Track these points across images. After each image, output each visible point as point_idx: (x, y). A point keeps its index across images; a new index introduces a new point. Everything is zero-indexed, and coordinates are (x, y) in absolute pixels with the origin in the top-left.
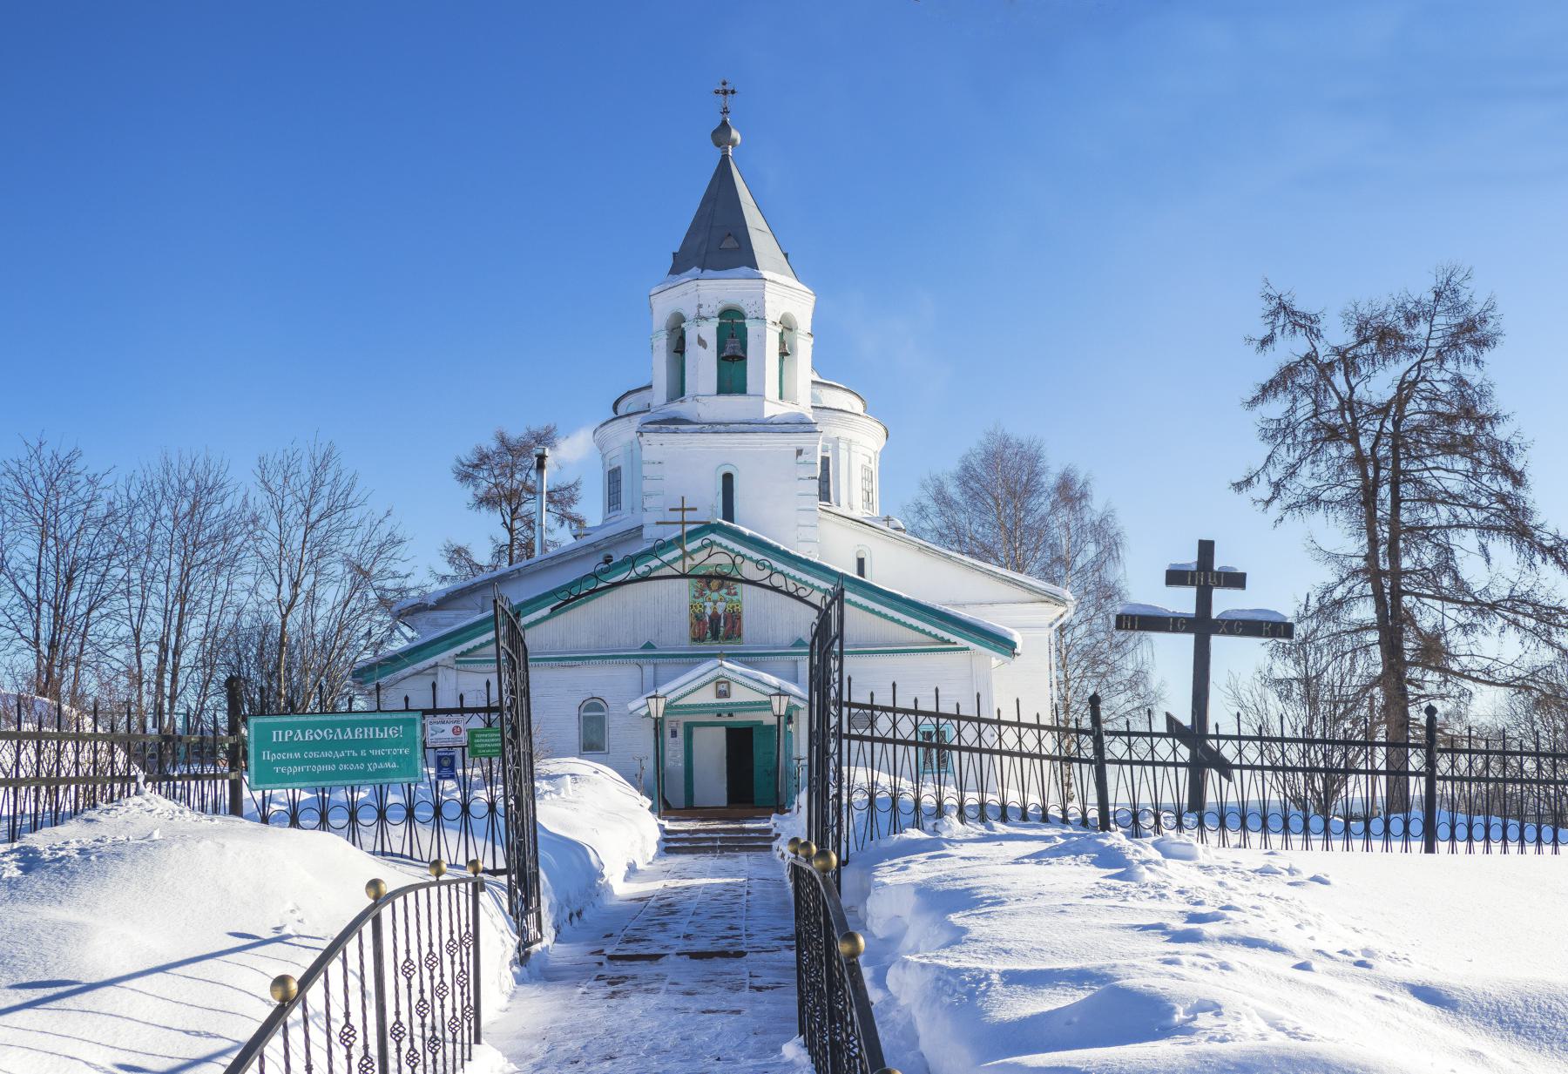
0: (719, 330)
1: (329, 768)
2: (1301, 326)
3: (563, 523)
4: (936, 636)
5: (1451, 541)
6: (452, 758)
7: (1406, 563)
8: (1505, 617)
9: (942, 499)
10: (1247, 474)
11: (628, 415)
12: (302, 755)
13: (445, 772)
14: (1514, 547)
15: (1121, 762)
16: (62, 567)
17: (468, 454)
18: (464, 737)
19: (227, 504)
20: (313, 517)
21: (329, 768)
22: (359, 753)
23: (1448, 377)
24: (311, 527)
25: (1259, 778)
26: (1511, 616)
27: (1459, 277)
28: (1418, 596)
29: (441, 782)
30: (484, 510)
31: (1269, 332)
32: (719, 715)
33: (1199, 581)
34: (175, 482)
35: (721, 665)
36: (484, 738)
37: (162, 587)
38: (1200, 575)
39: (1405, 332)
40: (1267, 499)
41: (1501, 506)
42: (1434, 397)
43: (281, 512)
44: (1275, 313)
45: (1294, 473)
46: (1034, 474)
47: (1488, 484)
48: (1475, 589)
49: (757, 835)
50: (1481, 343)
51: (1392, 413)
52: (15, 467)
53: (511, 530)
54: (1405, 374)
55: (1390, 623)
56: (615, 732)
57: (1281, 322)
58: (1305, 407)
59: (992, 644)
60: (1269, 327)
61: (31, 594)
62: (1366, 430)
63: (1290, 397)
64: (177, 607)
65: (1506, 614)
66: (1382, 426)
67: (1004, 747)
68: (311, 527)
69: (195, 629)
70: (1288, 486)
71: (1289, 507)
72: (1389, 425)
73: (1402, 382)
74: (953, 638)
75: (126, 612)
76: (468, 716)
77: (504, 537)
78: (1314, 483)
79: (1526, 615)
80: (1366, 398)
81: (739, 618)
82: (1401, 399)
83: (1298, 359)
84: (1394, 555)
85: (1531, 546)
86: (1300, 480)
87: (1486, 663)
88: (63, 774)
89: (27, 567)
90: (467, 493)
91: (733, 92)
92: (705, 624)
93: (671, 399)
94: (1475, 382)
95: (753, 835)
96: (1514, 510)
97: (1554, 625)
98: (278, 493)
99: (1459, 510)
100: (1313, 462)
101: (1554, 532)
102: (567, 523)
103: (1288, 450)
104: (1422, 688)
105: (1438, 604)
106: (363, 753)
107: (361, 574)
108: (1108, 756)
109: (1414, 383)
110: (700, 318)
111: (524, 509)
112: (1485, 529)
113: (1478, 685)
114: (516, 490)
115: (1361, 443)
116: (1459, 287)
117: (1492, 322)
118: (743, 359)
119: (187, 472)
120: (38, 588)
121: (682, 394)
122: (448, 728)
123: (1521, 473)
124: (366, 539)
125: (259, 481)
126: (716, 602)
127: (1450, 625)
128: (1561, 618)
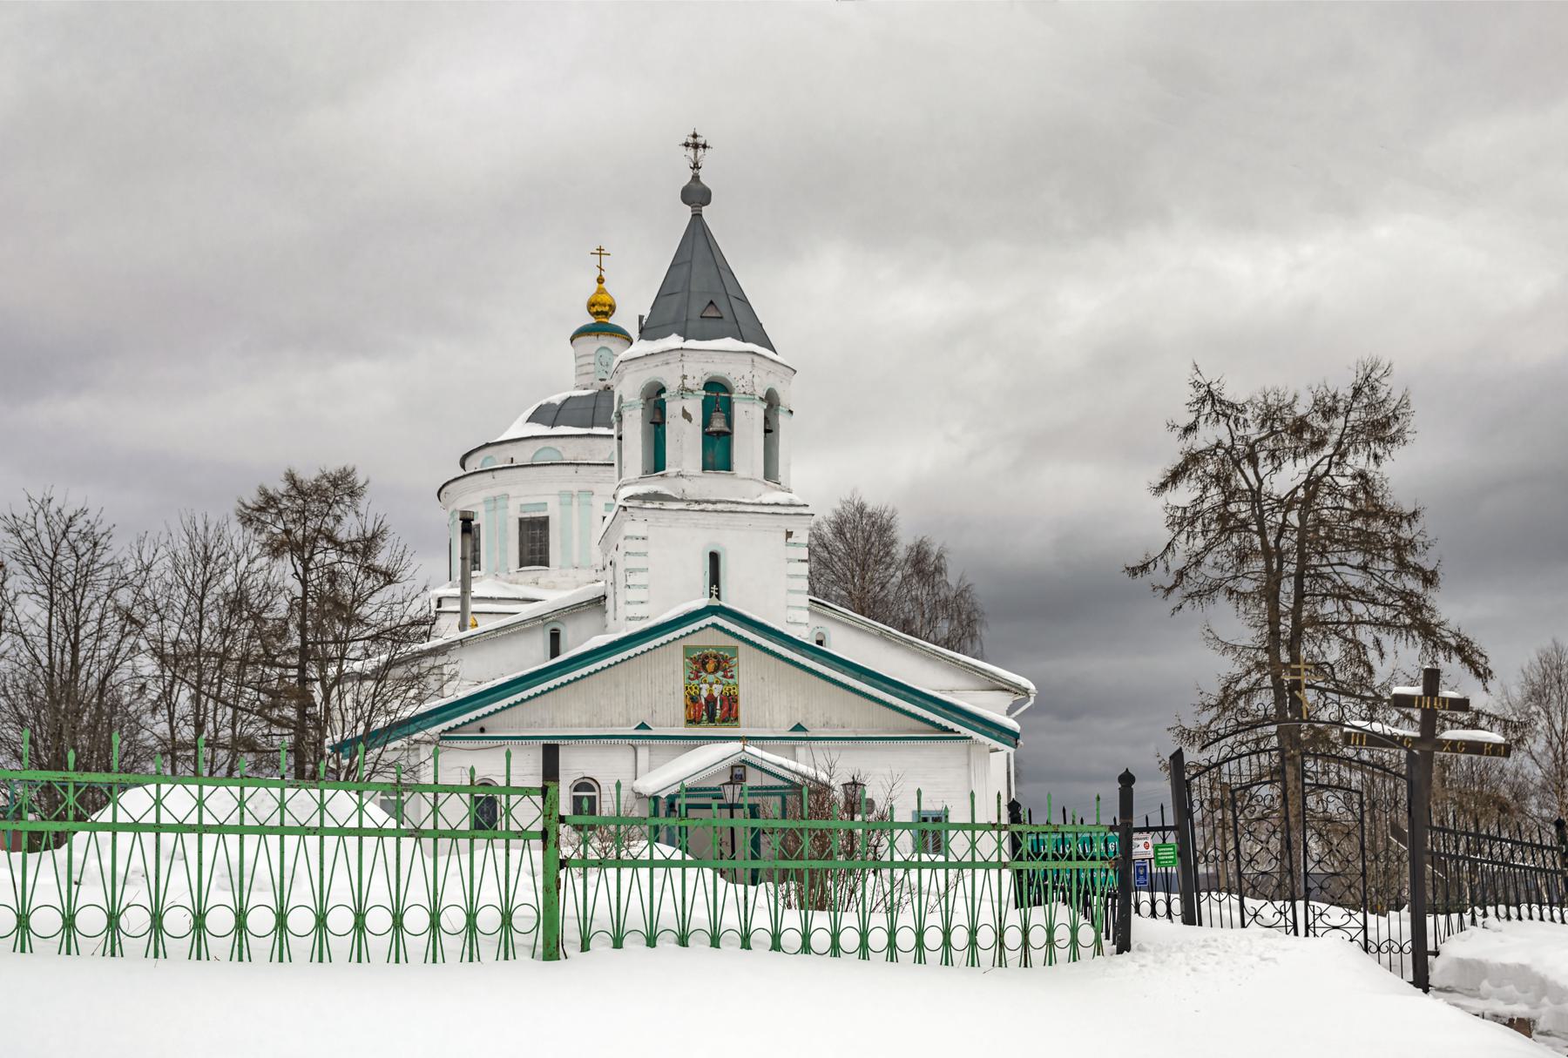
0: (706, 404)
2: (1225, 415)
17: (252, 498)
23: (1349, 471)
25: (501, 852)
27: (1379, 372)
33: (1426, 704)
35: (743, 750)
38: (1426, 699)
40: (1168, 585)
43: (354, 584)
44: (1203, 401)
46: (888, 545)
47: (1392, 581)
53: (304, 583)
55: (1289, 715)
59: (996, 734)
63: (1200, 485)
67: (969, 833)
70: (1192, 574)
71: (1190, 596)
72: (1293, 518)
74: (957, 727)
81: (736, 701)
85: (1435, 645)
86: (1202, 569)
91: (705, 146)
92: (701, 705)
101: (1455, 630)
110: (684, 391)
116: (1377, 384)
123: (1434, 573)
126: (711, 686)
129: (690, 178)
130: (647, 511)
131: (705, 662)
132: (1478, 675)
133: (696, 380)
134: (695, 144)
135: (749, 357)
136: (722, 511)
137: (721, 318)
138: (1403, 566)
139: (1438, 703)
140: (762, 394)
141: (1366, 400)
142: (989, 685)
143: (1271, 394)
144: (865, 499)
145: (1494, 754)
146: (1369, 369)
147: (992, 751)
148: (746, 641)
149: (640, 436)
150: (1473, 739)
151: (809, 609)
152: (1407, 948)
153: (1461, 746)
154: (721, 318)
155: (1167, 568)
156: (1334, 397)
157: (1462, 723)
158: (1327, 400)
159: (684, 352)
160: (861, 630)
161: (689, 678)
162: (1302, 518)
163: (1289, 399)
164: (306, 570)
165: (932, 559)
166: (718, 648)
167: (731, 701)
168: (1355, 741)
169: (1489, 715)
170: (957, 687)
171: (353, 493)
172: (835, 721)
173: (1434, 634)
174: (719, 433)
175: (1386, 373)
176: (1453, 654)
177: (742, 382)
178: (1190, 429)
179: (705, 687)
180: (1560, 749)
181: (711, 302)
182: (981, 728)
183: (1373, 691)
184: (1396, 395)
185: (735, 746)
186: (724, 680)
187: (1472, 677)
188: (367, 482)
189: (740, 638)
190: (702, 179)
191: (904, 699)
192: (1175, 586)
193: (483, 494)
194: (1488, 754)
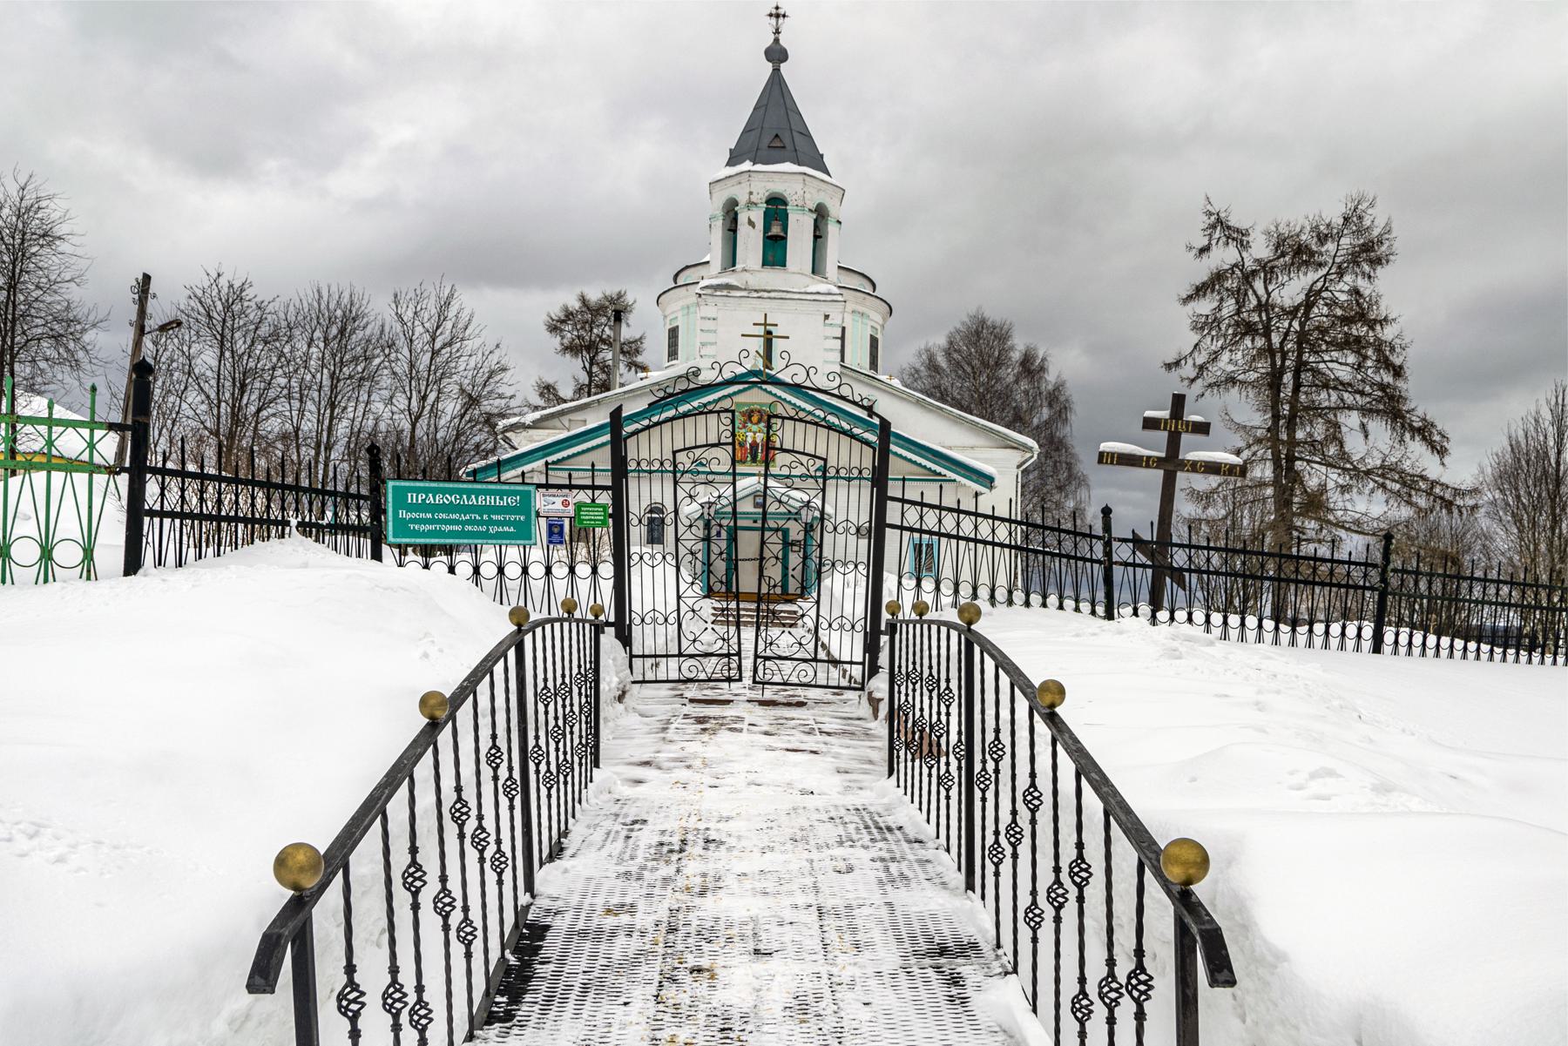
1: (456, 528)
2: (1233, 239)
3: (630, 370)
4: (930, 469)
5: (1339, 420)
6: (562, 526)
7: (1300, 435)
8: (1376, 482)
9: (933, 366)
10: (1177, 357)
12: (433, 515)
13: (555, 538)
14: (1389, 427)
15: (1126, 564)
16: (237, 375)
17: (557, 312)
18: (571, 510)
19: (368, 331)
20: (438, 345)
21: (456, 528)
23: (1346, 288)
24: (435, 353)
26: (1380, 480)
28: (1308, 462)
29: (551, 546)
30: (568, 356)
31: (1207, 243)
37: (316, 394)
39: (1315, 249)
40: (1192, 377)
41: (1380, 393)
42: (1332, 303)
43: (411, 340)
44: (1213, 227)
45: (1216, 358)
46: (1005, 351)
48: (1355, 458)
50: (1377, 262)
51: (1299, 315)
52: (199, 293)
53: (590, 374)
54: (1312, 285)
57: (1217, 235)
58: (1230, 306)
59: (975, 478)
60: (1207, 237)
61: (213, 395)
62: (1278, 328)
63: (1218, 298)
64: (328, 411)
65: (1377, 479)
66: (1290, 325)
68: (435, 353)
69: (342, 428)
70: (1210, 368)
71: (1210, 386)
72: (1296, 324)
73: (1310, 290)
74: (944, 471)
75: (288, 414)
76: (575, 491)
77: (584, 379)
78: (1231, 368)
79: (1393, 480)
80: (1278, 302)
82: (1309, 305)
83: (1227, 267)
84: (1291, 428)
85: (1403, 426)
87: (1357, 516)
88: (223, 513)
89: (209, 373)
90: (556, 341)
91: (784, 16)
93: (724, 270)
94: (1366, 293)
96: (1392, 398)
97: (1415, 489)
99: (1346, 395)
100: (1231, 351)
101: (1422, 416)
102: (633, 369)
103: (1212, 340)
104: (1304, 534)
105: (1323, 469)
106: (485, 517)
107: (472, 401)
108: (1115, 558)
109: (1320, 291)
110: (751, 204)
111: (601, 356)
112: (1366, 411)
113: (1349, 533)
114: (594, 342)
115: (1273, 337)
117: (1387, 244)
118: (784, 239)
120: (219, 390)
121: (734, 265)
122: (559, 500)
123: (1401, 367)
124: (479, 366)
125: (393, 315)
127: (1331, 485)
128: (1421, 484)
129: (772, 41)
133: (760, 196)
134: (777, 15)
135: (802, 177)
137: (784, 147)
140: (813, 207)
141: (1354, 228)
142: (1003, 444)
144: (987, 315)
145: (1230, 474)
149: (720, 241)
150: (1212, 460)
152: (858, 627)
153: (1201, 466)
154: (784, 147)
155: (1194, 364)
158: (1322, 228)
160: (902, 398)
164: (591, 364)
165: (1038, 361)
166: (761, 405)
169: (1442, 485)
173: (1403, 417)
175: (1372, 205)
177: (795, 197)
178: (1204, 250)
179: (750, 435)
181: (777, 136)
183: (1352, 463)
188: (635, 302)
190: (781, 42)
193: (681, 303)
194: (1224, 475)
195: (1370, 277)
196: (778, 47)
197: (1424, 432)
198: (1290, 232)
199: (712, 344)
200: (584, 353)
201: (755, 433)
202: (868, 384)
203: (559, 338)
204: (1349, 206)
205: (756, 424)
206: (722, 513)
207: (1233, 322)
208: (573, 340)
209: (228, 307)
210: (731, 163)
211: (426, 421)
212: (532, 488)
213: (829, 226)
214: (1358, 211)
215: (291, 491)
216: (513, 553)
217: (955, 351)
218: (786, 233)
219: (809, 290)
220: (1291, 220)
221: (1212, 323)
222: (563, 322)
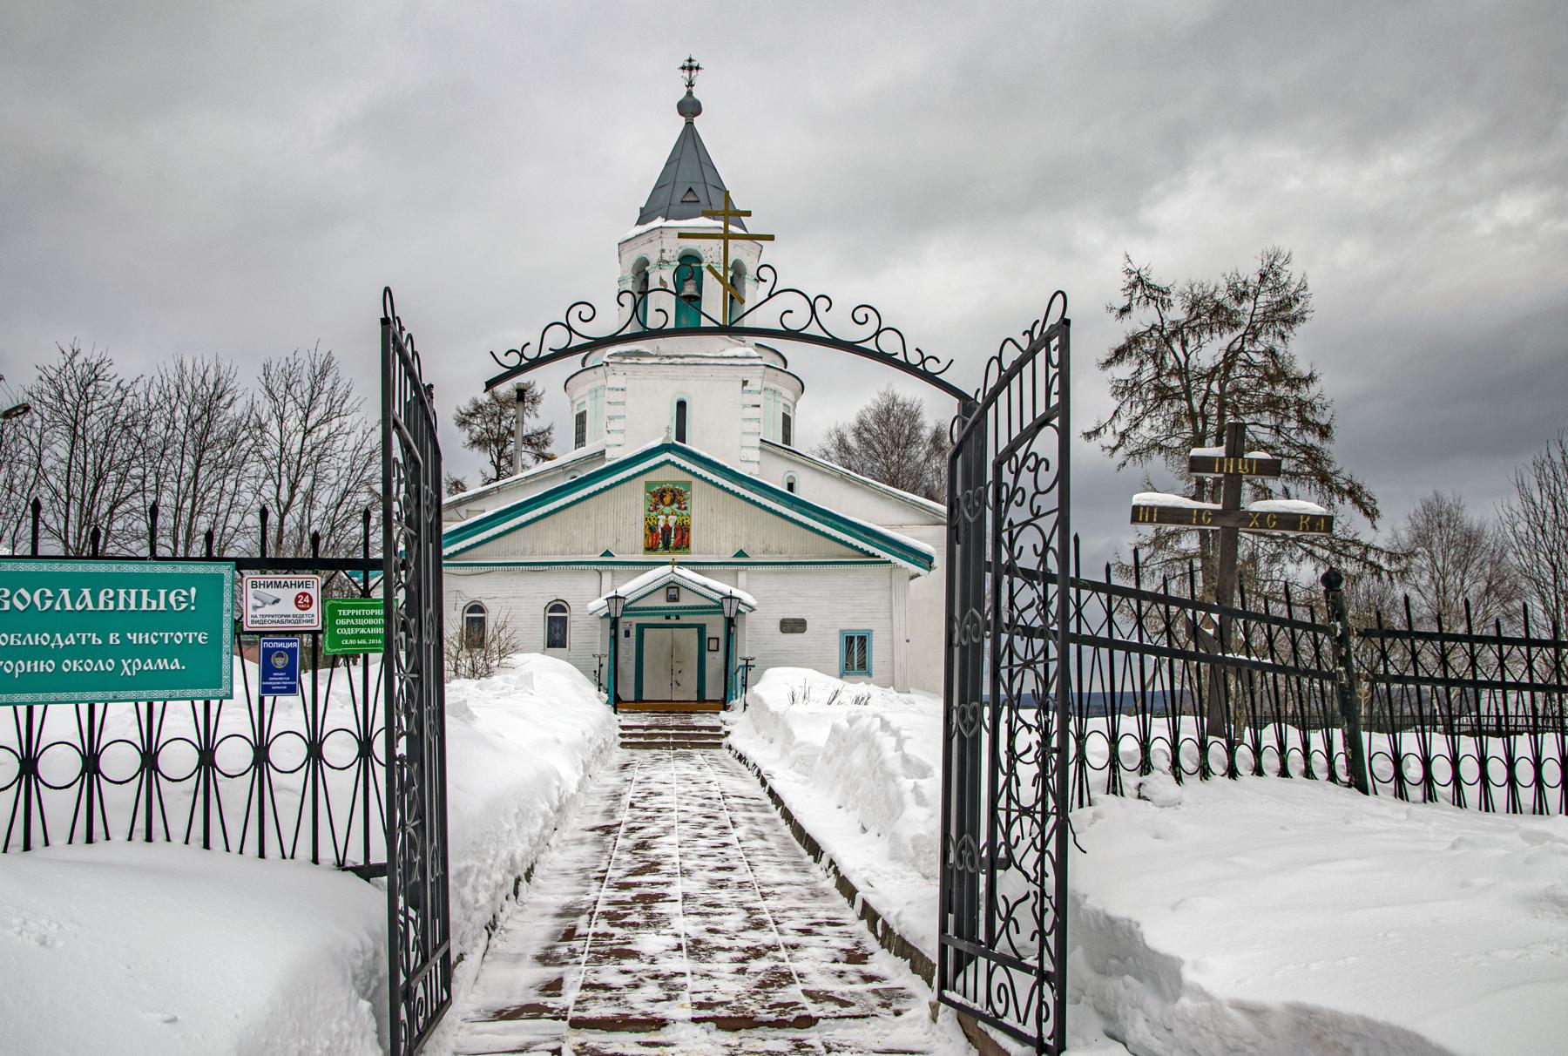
1: (41, 666)
2: (1154, 299)
3: (538, 460)
4: (862, 550)
9: (843, 446)
11: (594, 367)
13: (278, 679)
21: (41, 666)
22: (106, 639)
23: (1261, 349)
29: (268, 700)
30: (476, 449)
32: (668, 618)
33: (1228, 468)
34: (188, 388)
35: (673, 572)
36: (355, 617)
38: (1229, 462)
40: (1113, 445)
43: (282, 418)
44: (1134, 286)
45: (1138, 424)
46: (915, 429)
49: (707, 732)
50: (1291, 321)
56: (574, 635)
58: (1149, 370)
59: (912, 558)
60: (1128, 297)
63: (1138, 361)
65: (1306, 546)
70: (1132, 436)
71: (1132, 454)
72: (1215, 386)
73: (1228, 351)
74: (877, 552)
78: (1154, 434)
79: (1323, 547)
81: (688, 531)
91: (697, 68)
92: (658, 534)
95: (703, 732)
98: (281, 400)
102: (541, 460)
106: (113, 638)
110: (663, 263)
116: (1279, 271)
117: (1302, 301)
118: (698, 299)
119: (200, 379)
123: (1328, 426)
124: (359, 446)
125: (263, 388)
126: (667, 517)
130: (627, 366)
131: (664, 496)
132: (1367, 514)
136: (689, 364)
138: (1305, 424)
139: (1243, 466)
143: (1197, 286)
145: (1312, 529)
146: (1272, 258)
147: (912, 577)
148: (700, 477)
151: (761, 448)
155: (1114, 432)
156: (1245, 283)
157: (1354, 557)
158: (1239, 285)
159: (663, 230)
160: (825, 473)
161: (649, 510)
162: (1222, 387)
163: (1211, 289)
164: (499, 458)
166: (674, 483)
167: (684, 531)
168: (1144, 516)
169: (1376, 549)
170: (906, 521)
171: (534, 401)
172: (774, 548)
173: (1330, 480)
174: (690, 298)
175: (1287, 261)
176: (1346, 497)
177: (710, 253)
178: (1125, 310)
179: (662, 517)
180: (1441, 582)
181: (690, 190)
182: (899, 552)
184: (1296, 279)
185: (668, 568)
186: (679, 512)
187: (1362, 514)
188: (544, 392)
189: (695, 474)
190: (695, 95)
191: (831, 526)
192: (1119, 446)
193: (588, 387)
195: (1283, 337)
196: (690, 100)
197: (1354, 493)
198: (1204, 292)
199: (620, 417)
200: (493, 446)
201: (667, 516)
202: (789, 460)
203: (467, 432)
204: (1266, 262)
205: (669, 505)
206: (631, 609)
207: (1152, 387)
208: (482, 433)
209: (83, 386)
210: (640, 222)
211: (300, 511)
212: (226, 570)
213: (747, 285)
214: (1275, 268)
215: (1282, 627)
216: (179, 719)
217: (866, 430)
218: (701, 293)
219: (725, 354)
220: (1204, 281)
221: (1132, 388)
222: (472, 415)
